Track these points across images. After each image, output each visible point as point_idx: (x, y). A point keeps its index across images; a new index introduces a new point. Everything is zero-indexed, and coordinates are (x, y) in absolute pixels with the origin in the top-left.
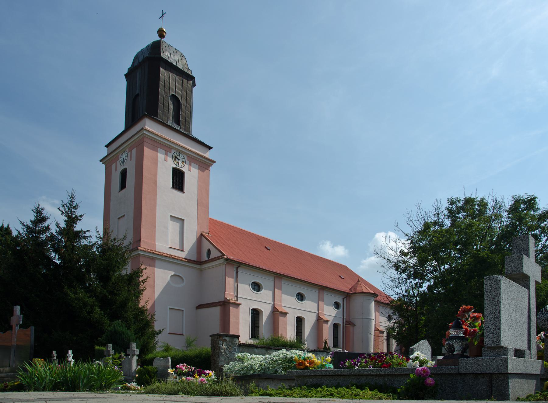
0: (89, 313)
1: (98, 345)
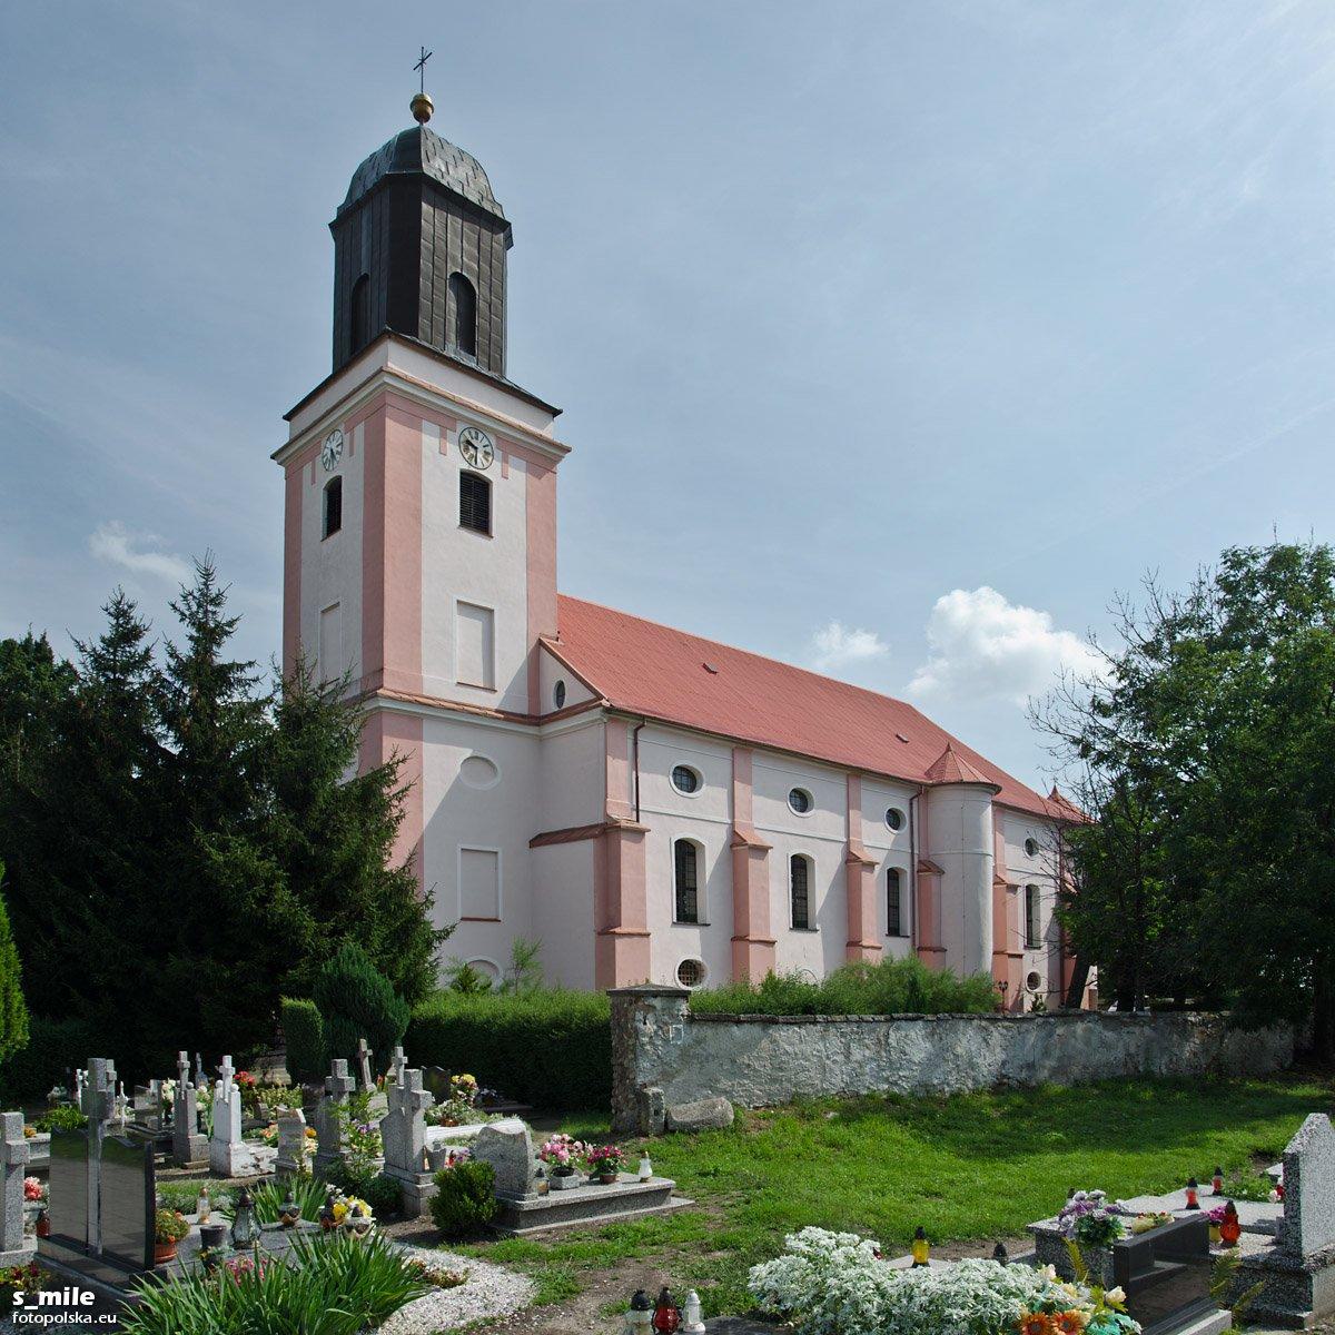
0: (262, 901)
1: (291, 996)
